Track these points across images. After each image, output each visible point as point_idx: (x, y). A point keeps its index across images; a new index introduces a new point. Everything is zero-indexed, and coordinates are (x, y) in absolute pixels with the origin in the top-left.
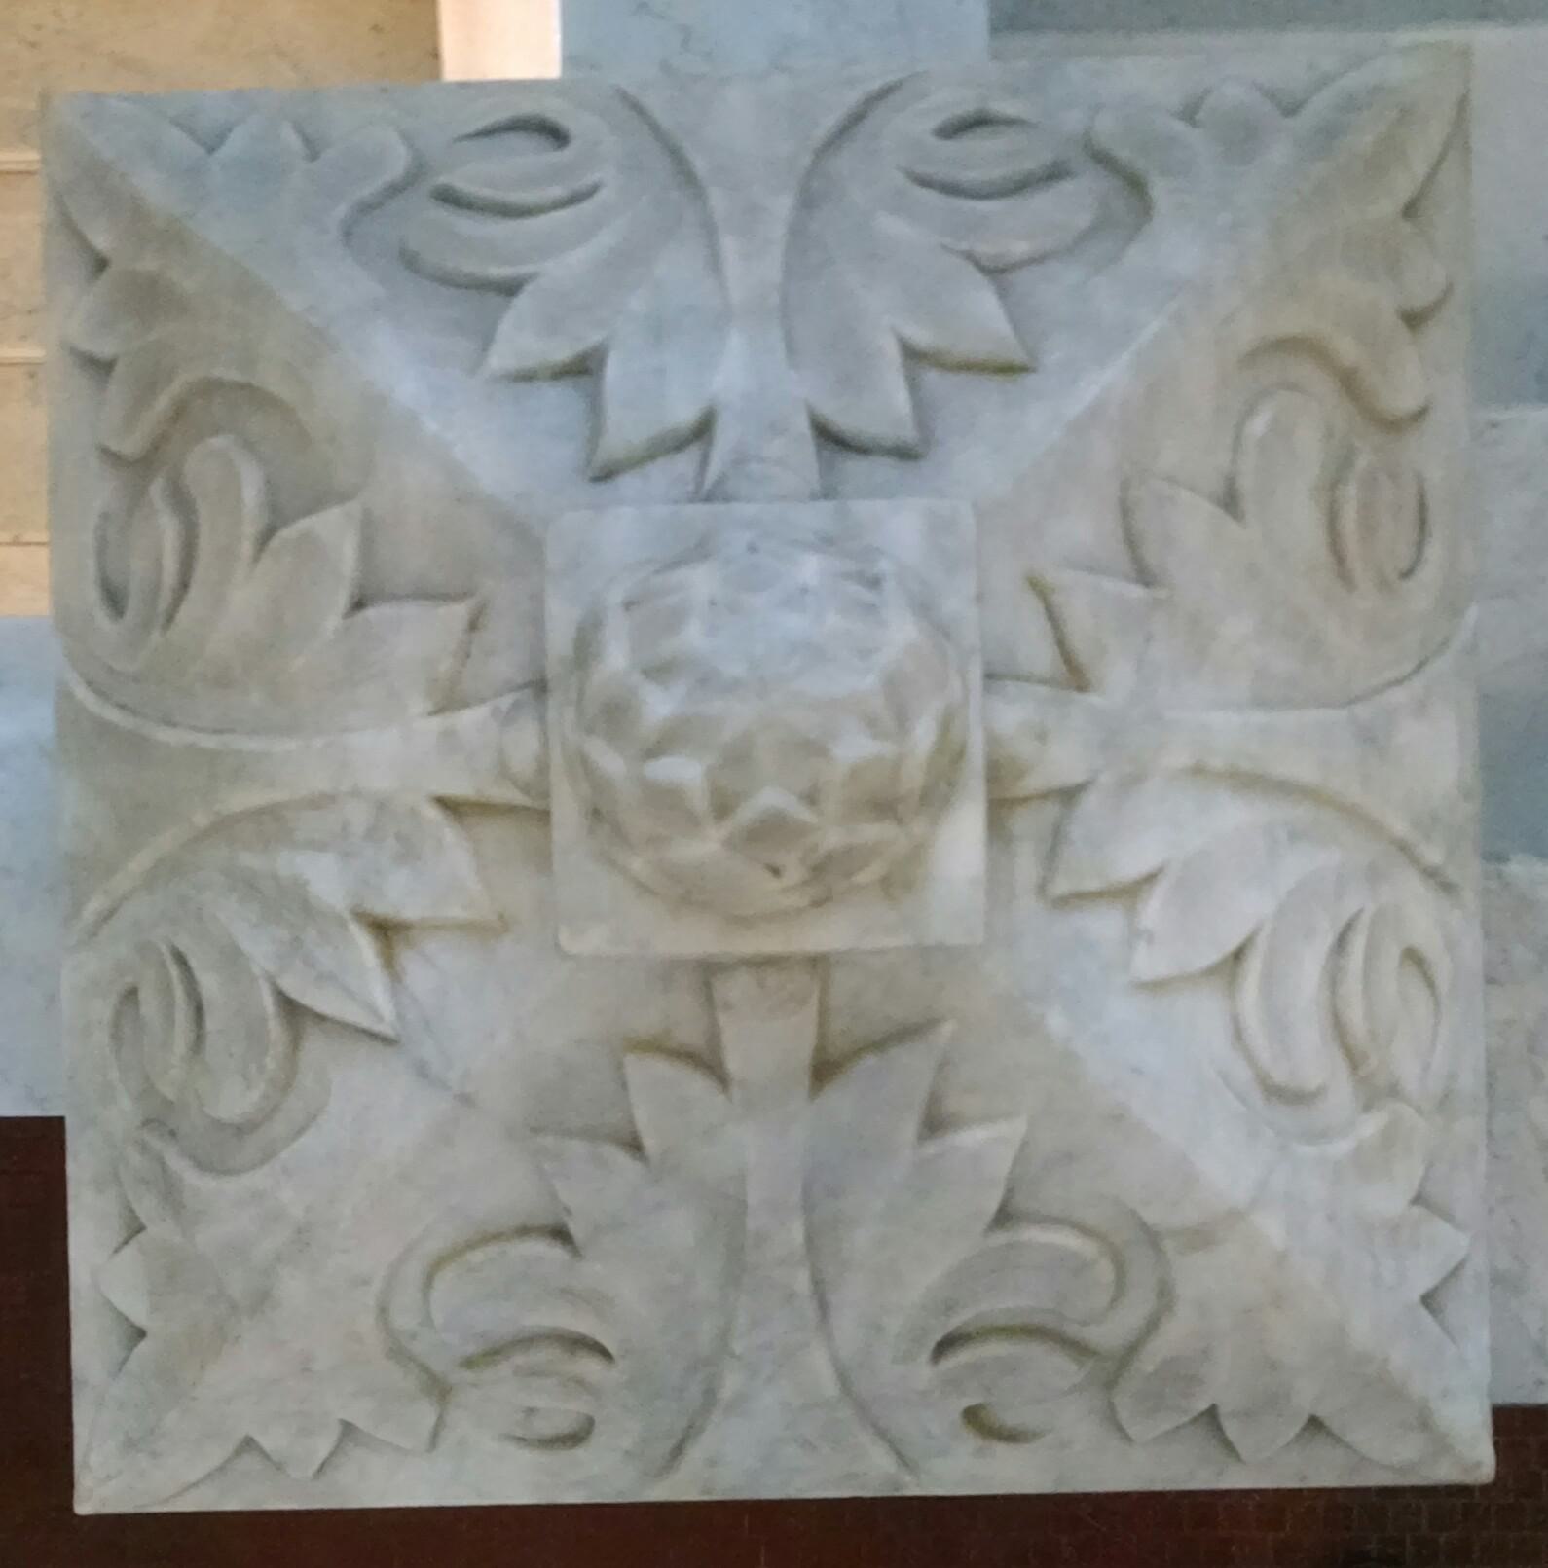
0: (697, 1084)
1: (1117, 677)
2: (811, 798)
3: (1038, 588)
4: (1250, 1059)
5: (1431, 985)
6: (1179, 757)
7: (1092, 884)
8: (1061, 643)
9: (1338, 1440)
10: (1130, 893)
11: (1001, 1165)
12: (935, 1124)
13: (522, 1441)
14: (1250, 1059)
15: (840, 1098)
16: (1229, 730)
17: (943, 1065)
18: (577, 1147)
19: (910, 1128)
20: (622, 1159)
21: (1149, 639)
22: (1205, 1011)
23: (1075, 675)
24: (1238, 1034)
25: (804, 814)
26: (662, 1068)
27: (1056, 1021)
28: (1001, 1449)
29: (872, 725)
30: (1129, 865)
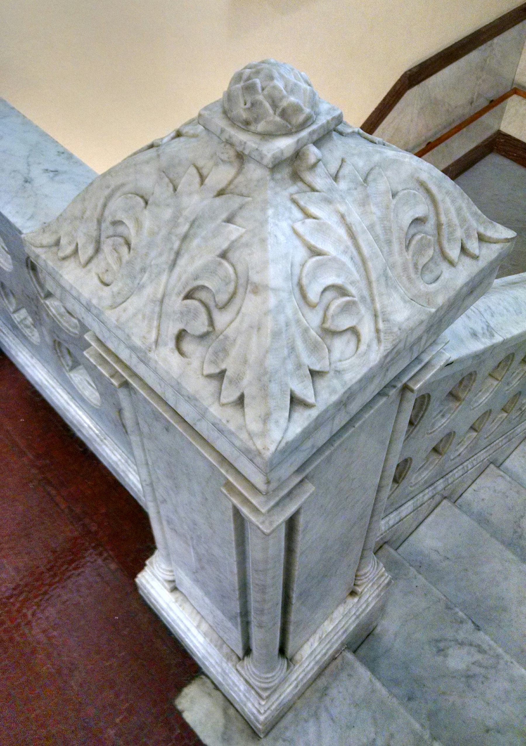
0: (197, 179)
1: (343, 185)
2: (263, 89)
3: (343, 161)
4: (301, 271)
5: (357, 348)
6: (342, 209)
7: (302, 203)
8: (338, 172)
9: (244, 415)
10: (308, 215)
11: (233, 237)
12: (229, 220)
13: (99, 278)
14: (301, 271)
15: (218, 201)
16: (355, 217)
17: (241, 207)
18: (167, 180)
19: (224, 216)
20: (171, 188)
21: (356, 189)
22: (301, 253)
23: (336, 178)
24: (303, 265)
25: (260, 90)
26: (195, 171)
27: (270, 212)
28: (177, 353)
29: (286, 87)
30: (313, 210)
